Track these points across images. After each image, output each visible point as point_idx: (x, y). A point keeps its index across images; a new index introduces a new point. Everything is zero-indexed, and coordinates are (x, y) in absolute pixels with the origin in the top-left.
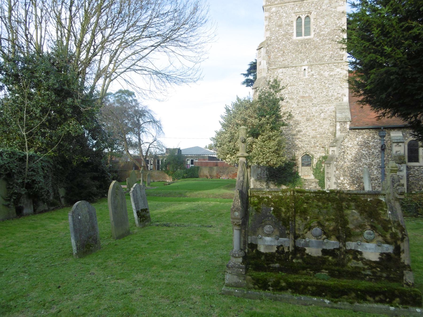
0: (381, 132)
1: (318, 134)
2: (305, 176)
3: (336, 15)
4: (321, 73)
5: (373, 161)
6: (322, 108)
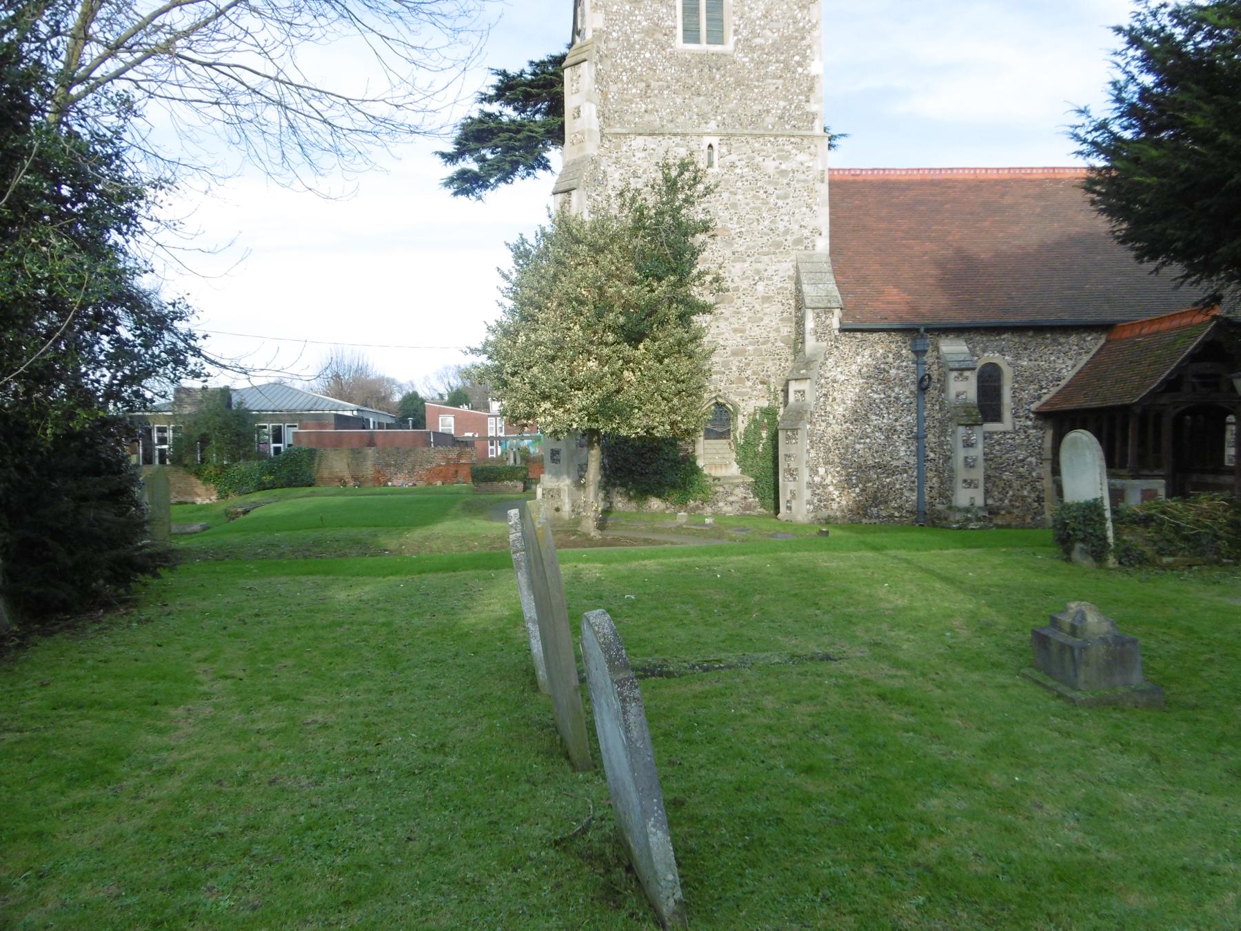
0: (918, 342)
1: (750, 343)
2: (716, 466)
4: (756, 161)
5: (896, 420)
6: (758, 266)
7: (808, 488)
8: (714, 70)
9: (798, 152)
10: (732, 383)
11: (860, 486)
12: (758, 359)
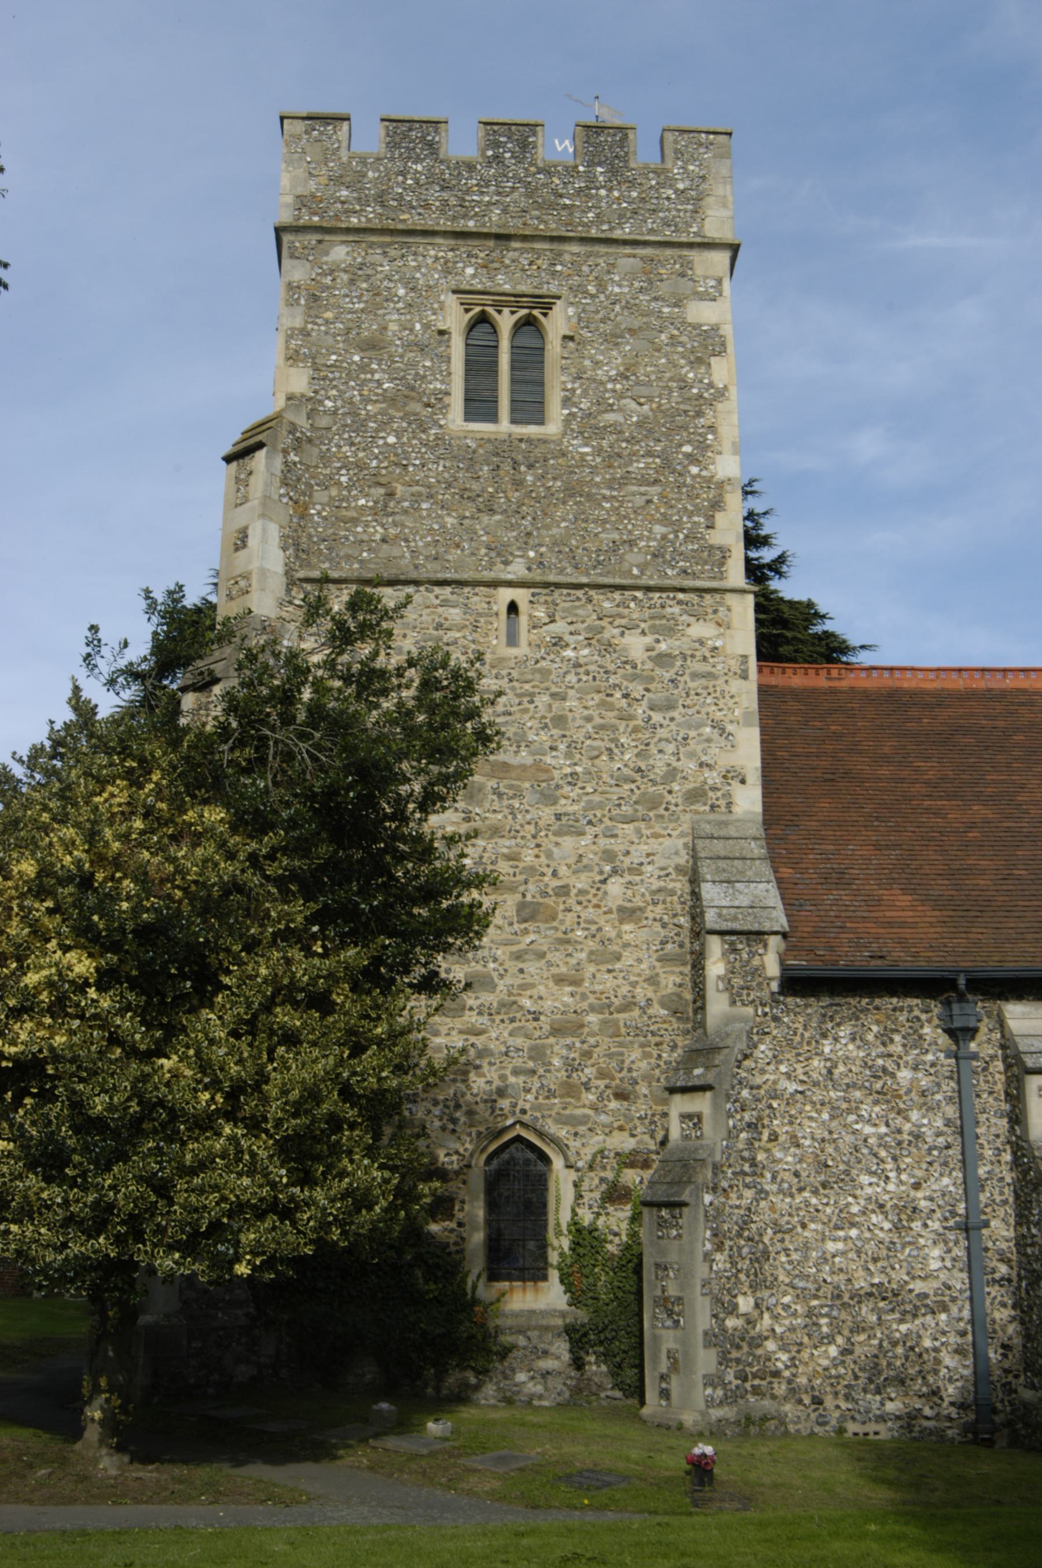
1: (592, 1009)
3: (684, 339)
4: (606, 635)
5: (917, 1186)
7: (707, 1345)
8: (523, 468)
9: (692, 620)
10: (551, 1094)
11: (840, 1340)
12: (606, 1042)
